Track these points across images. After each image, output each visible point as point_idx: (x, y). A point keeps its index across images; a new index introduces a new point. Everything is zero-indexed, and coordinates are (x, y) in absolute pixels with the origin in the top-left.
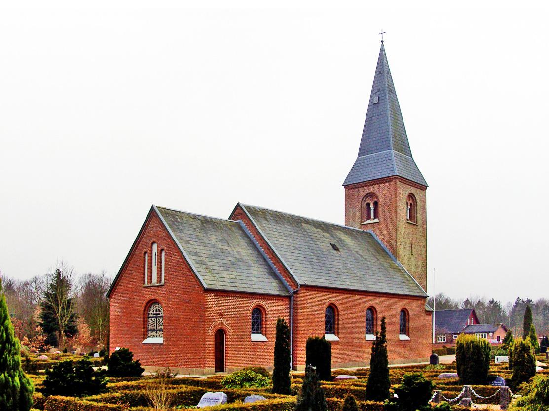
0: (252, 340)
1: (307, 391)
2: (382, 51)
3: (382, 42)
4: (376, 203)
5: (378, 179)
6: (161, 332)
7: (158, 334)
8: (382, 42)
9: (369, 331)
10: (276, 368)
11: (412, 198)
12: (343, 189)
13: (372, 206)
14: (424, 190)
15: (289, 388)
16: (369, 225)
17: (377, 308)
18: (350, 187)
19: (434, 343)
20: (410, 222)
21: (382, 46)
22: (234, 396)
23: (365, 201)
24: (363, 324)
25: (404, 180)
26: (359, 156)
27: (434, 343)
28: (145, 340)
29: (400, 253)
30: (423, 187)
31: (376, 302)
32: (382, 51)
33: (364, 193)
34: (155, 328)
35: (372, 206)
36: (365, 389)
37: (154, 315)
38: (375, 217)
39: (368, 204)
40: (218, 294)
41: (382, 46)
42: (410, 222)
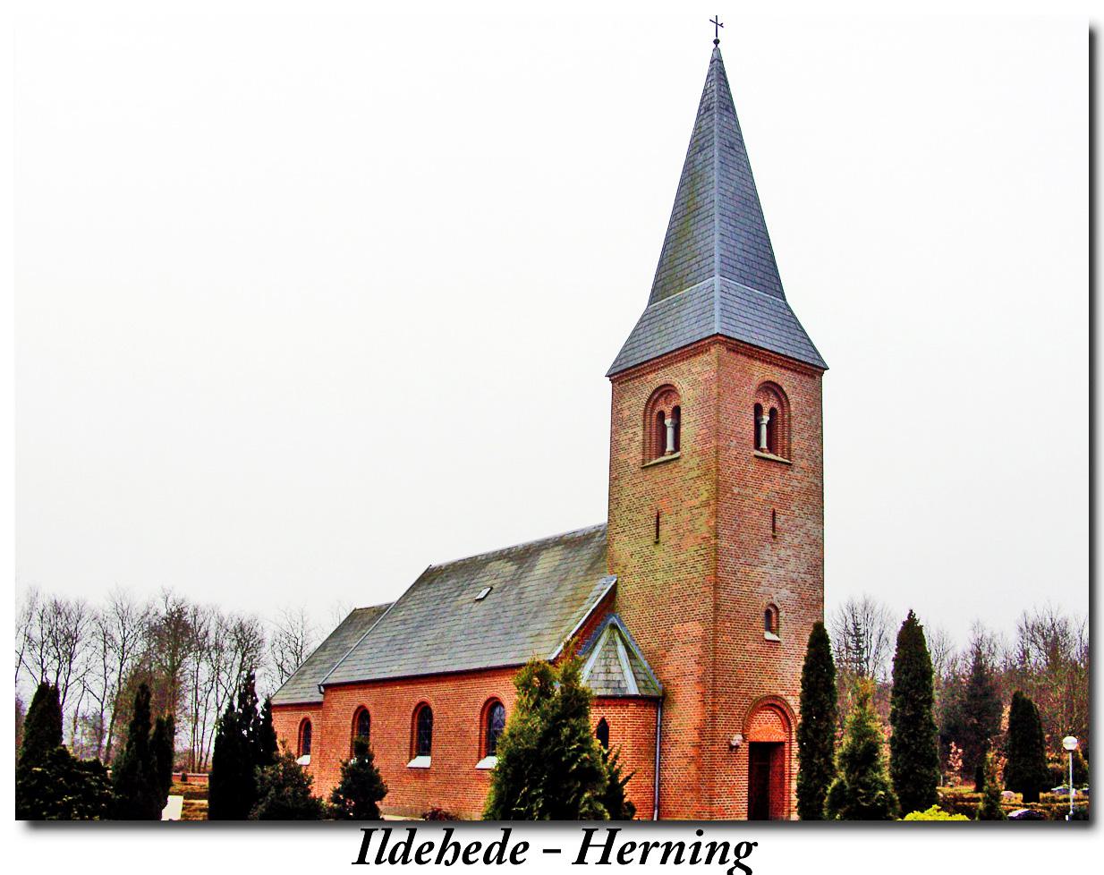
1: (826, 743)
3: (717, 42)
4: (677, 412)
8: (717, 42)
9: (490, 751)
10: (899, 653)
11: (776, 394)
12: (607, 385)
13: (668, 422)
14: (812, 376)
17: (433, 706)
18: (621, 376)
19: (655, 819)
20: (771, 456)
21: (717, 50)
24: (475, 731)
25: (634, 373)
26: (650, 304)
27: (655, 819)
29: (617, 554)
30: (813, 370)
31: (425, 693)
33: (648, 392)
35: (668, 422)
39: (662, 415)
41: (717, 50)
42: (771, 456)
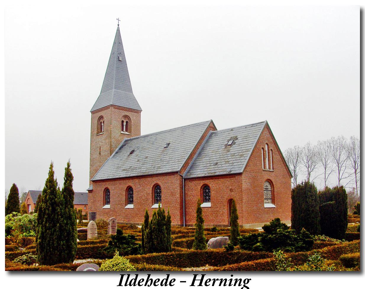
0: (210, 203)
2: (118, 31)
3: (118, 25)
5: (132, 109)
6: (269, 200)
7: (268, 202)
8: (118, 25)
15: (270, 226)
16: (125, 135)
22: (60, 235)
23: (99, 121)
28: (104, 206)
30: (138, 112)
32: (118, 31)
34: (267, 197)
35: (125, 124)
36: (348, 224)
37: (265, 189)
38: (126, 131)
40: (219, 177)
